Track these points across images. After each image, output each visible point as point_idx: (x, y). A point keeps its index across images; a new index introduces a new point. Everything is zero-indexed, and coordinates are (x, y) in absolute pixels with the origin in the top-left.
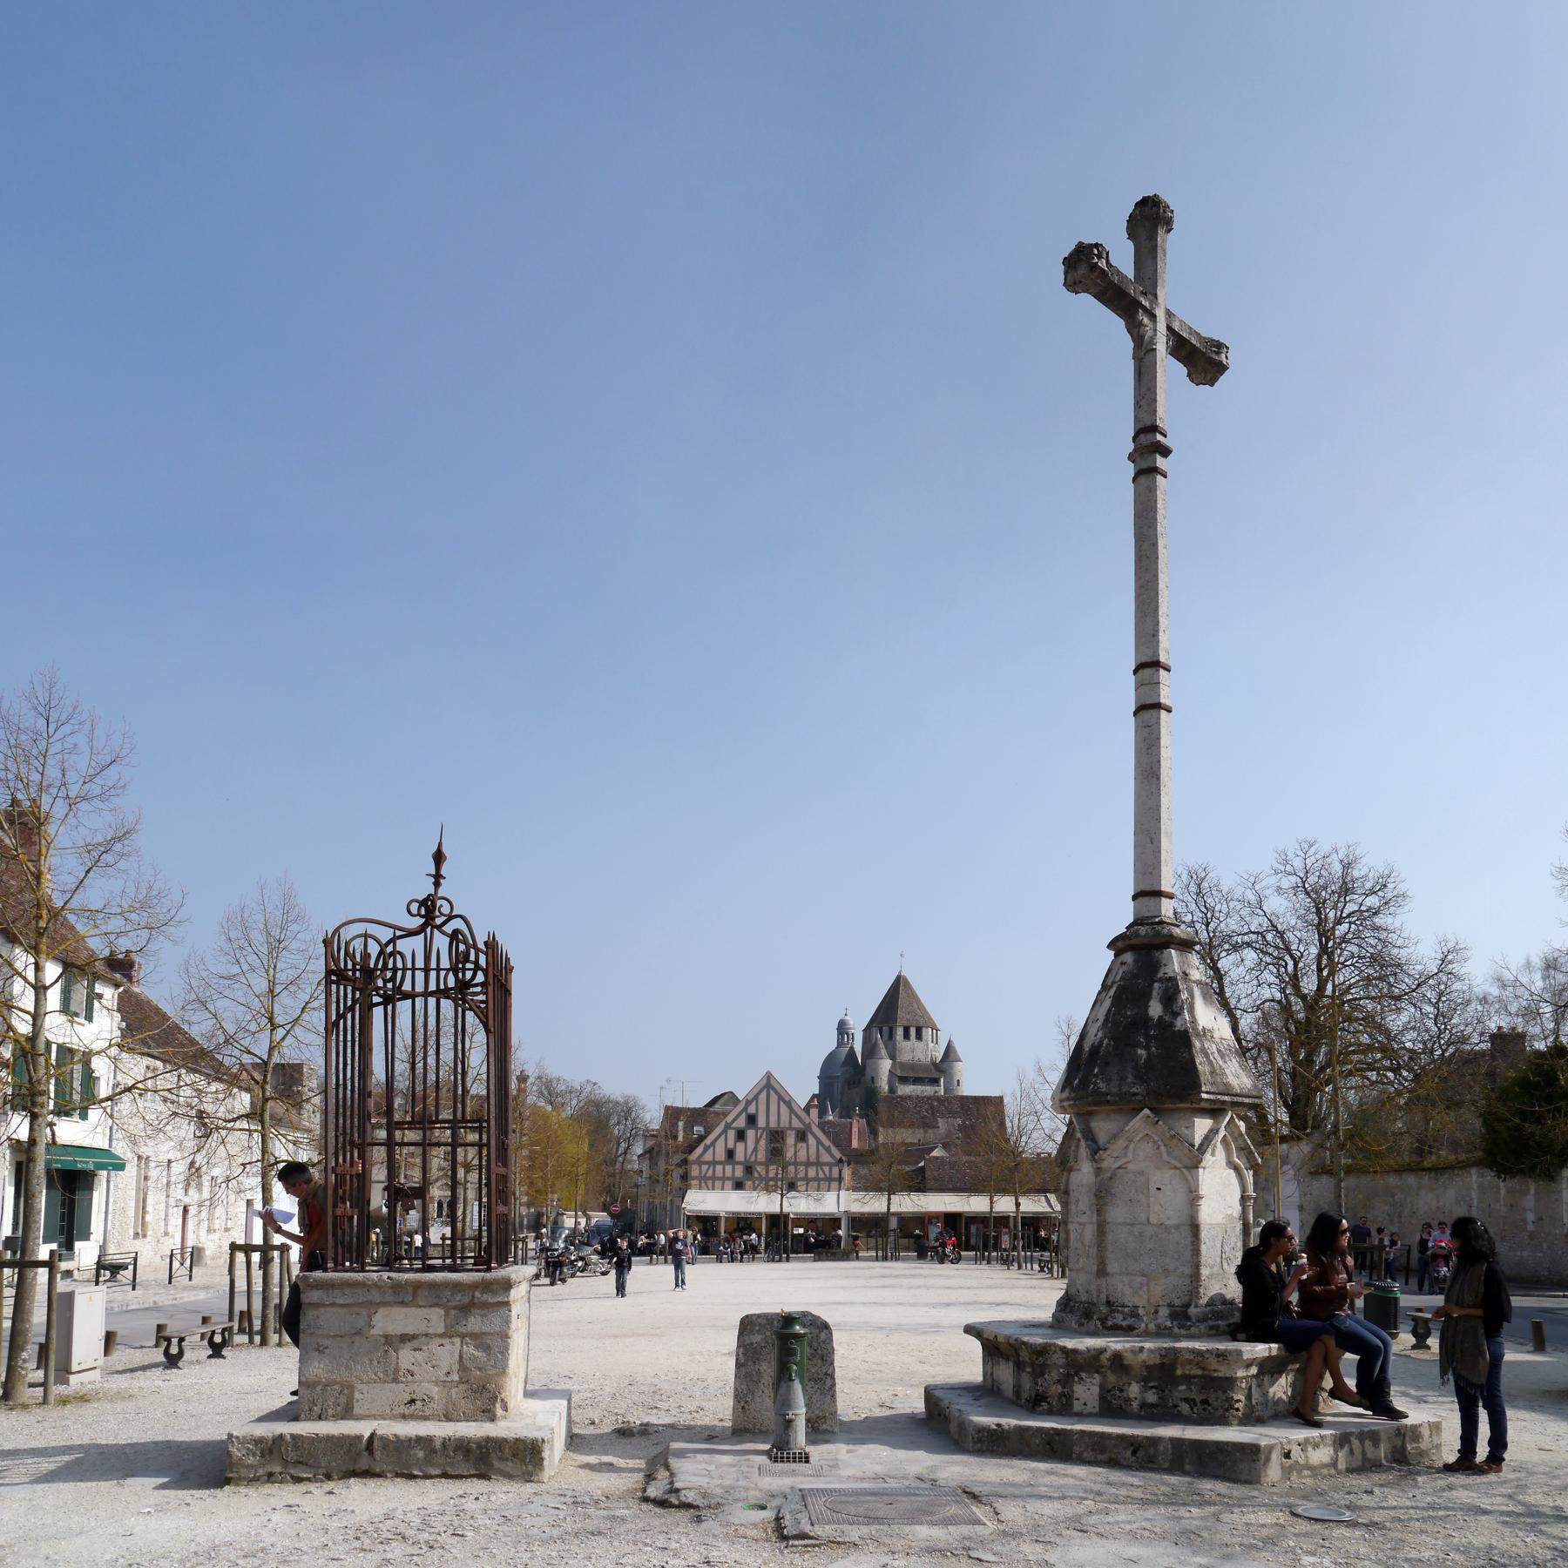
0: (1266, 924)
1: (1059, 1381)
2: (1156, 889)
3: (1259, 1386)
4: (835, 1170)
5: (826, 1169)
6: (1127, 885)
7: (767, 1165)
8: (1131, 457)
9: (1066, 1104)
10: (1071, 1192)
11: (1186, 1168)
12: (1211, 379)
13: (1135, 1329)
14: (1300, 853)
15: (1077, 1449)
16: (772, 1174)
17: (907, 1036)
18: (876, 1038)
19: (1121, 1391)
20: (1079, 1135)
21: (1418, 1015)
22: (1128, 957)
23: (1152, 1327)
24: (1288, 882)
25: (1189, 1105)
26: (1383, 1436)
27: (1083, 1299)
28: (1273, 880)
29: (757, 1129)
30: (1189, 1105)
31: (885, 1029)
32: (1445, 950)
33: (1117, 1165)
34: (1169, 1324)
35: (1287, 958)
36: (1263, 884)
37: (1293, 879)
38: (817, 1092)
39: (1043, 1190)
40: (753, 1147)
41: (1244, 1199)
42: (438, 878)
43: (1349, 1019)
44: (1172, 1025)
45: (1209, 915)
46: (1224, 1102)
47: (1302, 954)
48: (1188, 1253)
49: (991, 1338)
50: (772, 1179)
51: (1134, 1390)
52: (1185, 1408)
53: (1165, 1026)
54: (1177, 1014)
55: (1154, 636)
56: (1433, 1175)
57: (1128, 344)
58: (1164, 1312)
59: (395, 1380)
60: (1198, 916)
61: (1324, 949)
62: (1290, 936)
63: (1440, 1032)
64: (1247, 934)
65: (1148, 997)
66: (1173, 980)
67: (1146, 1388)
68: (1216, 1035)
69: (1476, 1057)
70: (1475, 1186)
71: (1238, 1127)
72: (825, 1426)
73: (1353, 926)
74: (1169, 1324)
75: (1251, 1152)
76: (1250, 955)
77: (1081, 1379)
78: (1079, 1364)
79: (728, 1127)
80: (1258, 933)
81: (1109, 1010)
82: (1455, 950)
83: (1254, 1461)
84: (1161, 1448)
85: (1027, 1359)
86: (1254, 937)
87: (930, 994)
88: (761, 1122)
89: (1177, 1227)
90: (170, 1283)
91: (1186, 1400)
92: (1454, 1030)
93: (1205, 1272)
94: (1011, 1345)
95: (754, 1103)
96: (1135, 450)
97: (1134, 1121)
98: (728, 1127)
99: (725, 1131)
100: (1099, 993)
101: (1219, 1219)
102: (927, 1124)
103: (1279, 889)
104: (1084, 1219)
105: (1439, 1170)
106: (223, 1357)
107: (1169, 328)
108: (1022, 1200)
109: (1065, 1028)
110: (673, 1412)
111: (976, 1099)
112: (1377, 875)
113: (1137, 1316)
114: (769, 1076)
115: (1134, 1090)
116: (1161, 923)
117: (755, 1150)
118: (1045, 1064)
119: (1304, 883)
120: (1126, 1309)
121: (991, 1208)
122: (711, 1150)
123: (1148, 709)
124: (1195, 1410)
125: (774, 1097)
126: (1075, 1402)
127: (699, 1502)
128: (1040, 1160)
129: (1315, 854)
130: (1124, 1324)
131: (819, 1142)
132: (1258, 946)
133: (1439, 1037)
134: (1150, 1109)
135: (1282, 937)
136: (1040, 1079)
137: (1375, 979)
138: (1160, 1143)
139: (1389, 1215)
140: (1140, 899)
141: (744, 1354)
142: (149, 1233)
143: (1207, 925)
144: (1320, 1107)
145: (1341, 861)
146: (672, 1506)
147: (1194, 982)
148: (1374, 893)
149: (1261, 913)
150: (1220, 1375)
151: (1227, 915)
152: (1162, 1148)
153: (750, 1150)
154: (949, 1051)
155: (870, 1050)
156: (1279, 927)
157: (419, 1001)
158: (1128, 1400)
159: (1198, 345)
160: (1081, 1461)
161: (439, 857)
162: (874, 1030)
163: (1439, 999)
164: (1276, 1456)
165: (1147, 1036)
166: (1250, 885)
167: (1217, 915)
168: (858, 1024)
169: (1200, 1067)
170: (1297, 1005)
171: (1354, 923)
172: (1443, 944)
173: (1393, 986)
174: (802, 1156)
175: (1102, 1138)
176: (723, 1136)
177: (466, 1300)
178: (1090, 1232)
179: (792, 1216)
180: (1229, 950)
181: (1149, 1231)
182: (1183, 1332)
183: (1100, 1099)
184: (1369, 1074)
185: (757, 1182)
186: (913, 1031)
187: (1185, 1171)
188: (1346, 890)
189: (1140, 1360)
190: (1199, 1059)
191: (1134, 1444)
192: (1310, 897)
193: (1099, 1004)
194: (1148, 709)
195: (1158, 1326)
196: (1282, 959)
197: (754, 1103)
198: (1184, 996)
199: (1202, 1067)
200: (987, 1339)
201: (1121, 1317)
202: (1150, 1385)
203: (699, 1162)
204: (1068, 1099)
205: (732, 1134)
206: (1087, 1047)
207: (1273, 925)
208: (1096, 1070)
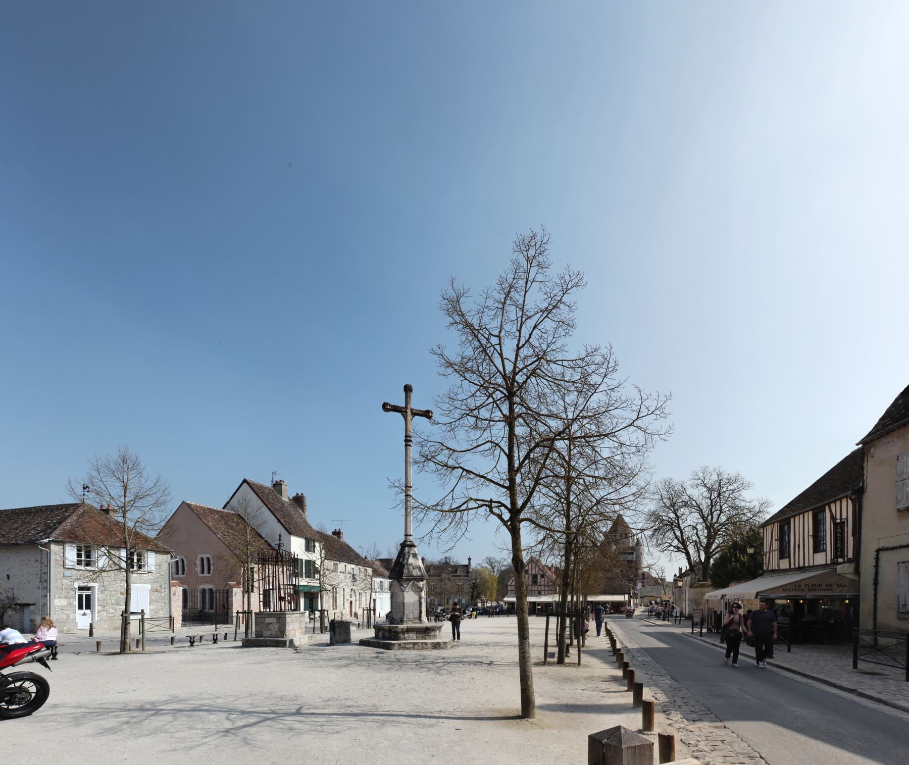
5: (551, 587)
51: (387, 634)
53: (402, 563)
88: (530, 572)
142: (338, 608)
169: (404, 571)
174: (543, 583)
181: (398, 604)
186: (624, 535)
203: (510, 585)
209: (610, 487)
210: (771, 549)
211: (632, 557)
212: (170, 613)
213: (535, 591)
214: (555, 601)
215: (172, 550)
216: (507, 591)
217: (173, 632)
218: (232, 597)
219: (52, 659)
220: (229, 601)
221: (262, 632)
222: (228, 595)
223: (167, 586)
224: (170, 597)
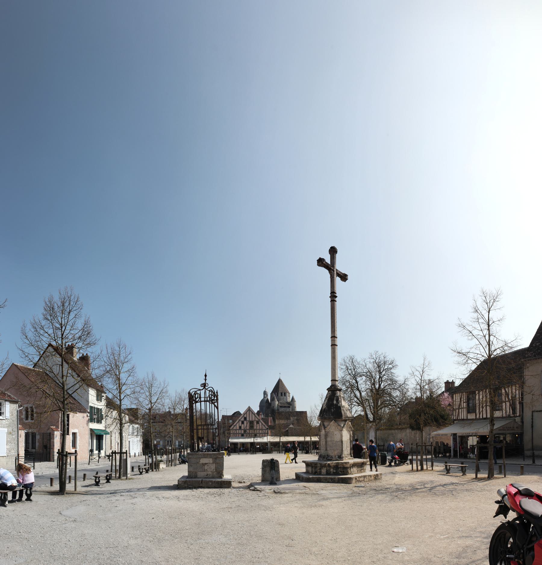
0: (367, 371)
4: (266, 431)
5: (264, 431)
6: (330, 378)
7: (250, 429)
15: (322, 480)
17: (282, 395)
22: (330, 392)
23: (335, 459)
26: (372, 476)
28: (369, 360)
29: (247, 421)
31: (276, 393)
36: (367, 361)
37: (373, 360)
38: (259, 410)
39: (316, 435)
40: (246, 425)
41: (350, 436)
42: (206, 379)
43: (386, 394)
44: (338, 405)
48: (341, 446)
51: (332, 470)
52: (340, 472)
53: (336, 405)
54: (339, 403)
57: (329, 275)
58: (337, 456)
59: (204, 471)
60: (352, 368)
61: (380, 377)
66: (338, 397)
67: (334, 470)
68: (346, 407)
76: (364, 378)
78: (323, 466)
79: (239, 420)
87: (288, 385)
88: (248, 419)
89: (339, 441)
90: (89, 464)
91: (340, 471)
93: (344, 449)
98: (239, 420)
99: (239, 422)
102: (288, 419)
103: (370, 362)
104: (323, 440)
105: (401, 429)
106: (110, 482)
107: (337, 273)
108: (312, 437)
111: (300, 412)
113: (332, 457)
114: (249, 407)
115: (331, 417)
116: (336, 386)
123: (334, 345)
125: (251, 413)
127: (260, 490)
128: (315, 428)
131: (262, 424)
136: (316, 409)
140: (333, 381)
143: (354, 370)
146: (255, 490)
153: (245, 426)
154: (293, 399)
155: (272, 399)
157: (203, 403)
158: (331, 472)
160: (323, 482)
161: (206, 376)
162: (273, 393)
164: (354, 479)
165: (334, 407)
168: (269, 392)
174: (258, 428)
175: (326, 426)
176: (238, 423)
177: (216, 457)
178: (324, 443)
181: (334, 442)
183: (325, 418)
186: (283, 394)
188: (385, 363)
190: (342, 411)
191: (332, 479)
194: (334, 345)
198: (340, 400)
199: (343, 413)
203: (233, 429)
205: (240, 422)
206: (323, 409)
209: (374, 356)
210: (460, 407)
211: (289, 410)
212: (18, 452)
213: (239, 434)
214: (269, 442)
215: (19, 400)
216: (230, 434)
217: (34, 469)
218: (54, 439)
219: (26, 500)
220: (51, 443)
221: (196, 473)
222: (50, 437)
223: (16, 430)
224: (18, 438)
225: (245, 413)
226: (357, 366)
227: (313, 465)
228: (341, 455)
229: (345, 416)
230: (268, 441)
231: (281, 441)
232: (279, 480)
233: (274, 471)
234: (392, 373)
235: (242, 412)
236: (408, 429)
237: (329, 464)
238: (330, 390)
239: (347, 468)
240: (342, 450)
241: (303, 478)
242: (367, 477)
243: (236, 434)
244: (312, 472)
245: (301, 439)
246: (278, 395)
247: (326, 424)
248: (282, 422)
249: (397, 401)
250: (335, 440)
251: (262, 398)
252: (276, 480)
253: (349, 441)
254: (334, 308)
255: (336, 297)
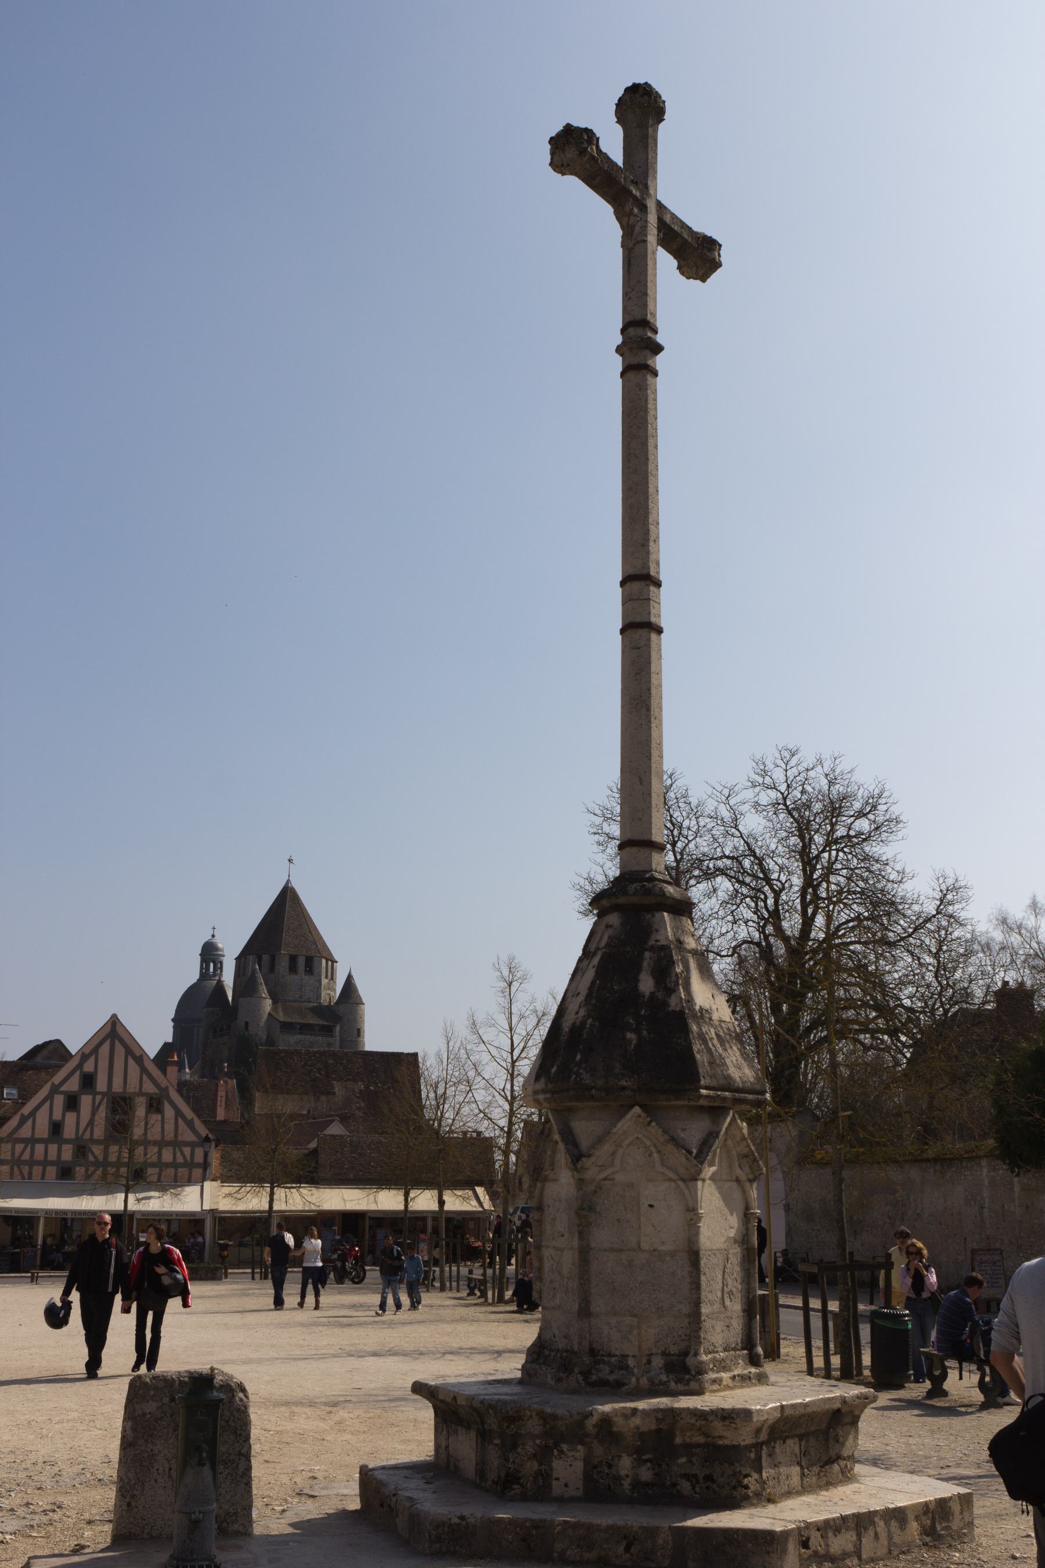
1: (535, 1455)
2: (646, 838)
3: (770, 1455)
4: (199, 1153)
5: (187, 1151)
8: (619, 350)
9: (541, 1097)
10: (546, 1209)
11: (683, 1180)
12: (703, 275)
13: (624, 1384)
14: (779, 762)
15: (559, 1546)
16: (113, 1158)
17: (293, 968)
18: (254, 971)
19: (610, 1466)
20: (556, 1137)
21: (915, 965)
22: (614, 919)
23: (644, 1381)
24: (767, 797)
25: (685, 1103)
26: (911, 1516)
27: (560, 1346)
28: (749, 794)
29: (95, 1094)
30: (685, 1103)
31: (265, 958)
32: (944, 887)
33: (603, 1175)
34: (664, 1378)
35: (767, 888)
36: (738, 798)
37: (773, 795)
38: (170, 1040)
39: (469, 1184)
44: (665, 1004)
45: (676, 832)
46: (724, 1099)
47: (783, 885)
49: (449, 1400)
50: (113, 1165)
51: (625, 1464)
52: (685, 1486)
54: (671, 991)
55: (643, 545)
56: (938, 1167)
58: (658, 1362)
61: (809, 883)
62: (770, 864)
63: (943, 989)
64: (721, 858)
65: (639, 969)
66: (665, 948)
67: (639, 1462)
68: (715, 1016)
69: (979, 1016)
70: (986, 1182)
71: (741, 1129)
72: (236, 1527)
73: (841, 854)
74: (664, 1378)
75: (755, 1160)
76: (724, 885)
77: (562, 1452)
79: (55, 1090)
80: (732, 858)
81: (593, 983)
82: (955, 889)
83: (768, 1553)
84: (660, 1541)
85: (495, 1427)
86: (728, 862)
88: (101, 1085)
89: (673, 1254)
91: (687, 1477)
92: (957, 987)
93: (705, 1310)
94: (475, 1410)
95: (92, 1058)
96: (624, 343)
97: (623, 1121)
98: (55, 1090)
99: (50, 1097)
100: (580, 960)
101: (720, 1243)
103: (756, 805)
105: (943, 1161)
107: (661, 221)
109: (506, 973)
110: (21, 1512)
112: (866, 794)
113: (626, 1368)
114: (114, 1021)
115: (623, 1083)
116: (653, 879)
117: (91, 1123)
118: (480, 1018)
119: (785, 799)
120: (613, 1360)
121: (406, 1206)
122: (30, 1122)
124: (697, 1489)
125: (120, 1050)
126: (554, 1483)
129: (797, 765)
130: (611, 1378)
131: (178, 1113)
132: (732, 874)
133: (940, 994)
134: (641, 1106)
135: (760, 864)
137: (867, 919)
138: (652, 1148)
139: (889, 1218)
141: (134, 1429)
144: (805, 1075)
145: (827, 775)
147: (690, 952)
148: (865, 815)
149: (737, 833)
150: (727, 1442)
151: (697, 833)
152: (655, 1155)
153: (83, 1124)
154: (349, 982)
156: (757, 851)
158: (617, 1479)
159: (690, 240)
162: (251, 958)
163: (940, 949)
164: (792, 1547)
166: (724, 798)
167: (685, 832)
168: (231, 948)
169: (698, 1056)
170: (780, 949)
171: (842, 850)
172: (941, 880)
173: (887, 929)
174: (155, 1134)
175: (585, 1143)
176: (48, 1103)
178: (569, 1260)
179: (138, 1216)
180: (699, 876)
182: (681, 1387)
184: (862, 1037)
185: (92, 1169)
186: (301, 961)
187: (680, 1183)
189: (632, 1426)
190: (697, 1046)
192: (793, 817)
193: (580, 974)
195: (651, 1381)
196: (759, 890)
197: (92, 1058)
198: (679, 968)
200: (442, 1401)
201: (607, 1369)
202: (644, 1457)
204: (543, 1091)
205: (59, 1100)
206: (566, 1026)
207: (750, 849)
208: (578, 1057)
209: (779, 775)
211: (329, 1044)
213: (45, 1163)
225: (91, 1050)
226: (686, 823)
227: (492, 1422)
228: (686, 1354)
229: (713, 1076)
230: (206, 1207)
231: (276, 1207)
232: (246, 1532)
233: (207, 1470)
234: (866, 858)
235: (74, 1046)
236: (984, 1163)
237: (606, 1421)
238: (616, 908)
239: (731, 1454)
240: (695, 1317)
241: (415, 1519)
242: (881, 1524)
243: (32, 1163)
244: (481, 1471)
245: (389, 1200)
246: (272, 968)
247: (584, 1128)
248: (288, 1105)
249: (902, 1006)
250: (645, 1246)
251: (193, 976)
252: (223, 1532)
253: (736, 1252)
254: (646, 410)
255: (658, 349)
